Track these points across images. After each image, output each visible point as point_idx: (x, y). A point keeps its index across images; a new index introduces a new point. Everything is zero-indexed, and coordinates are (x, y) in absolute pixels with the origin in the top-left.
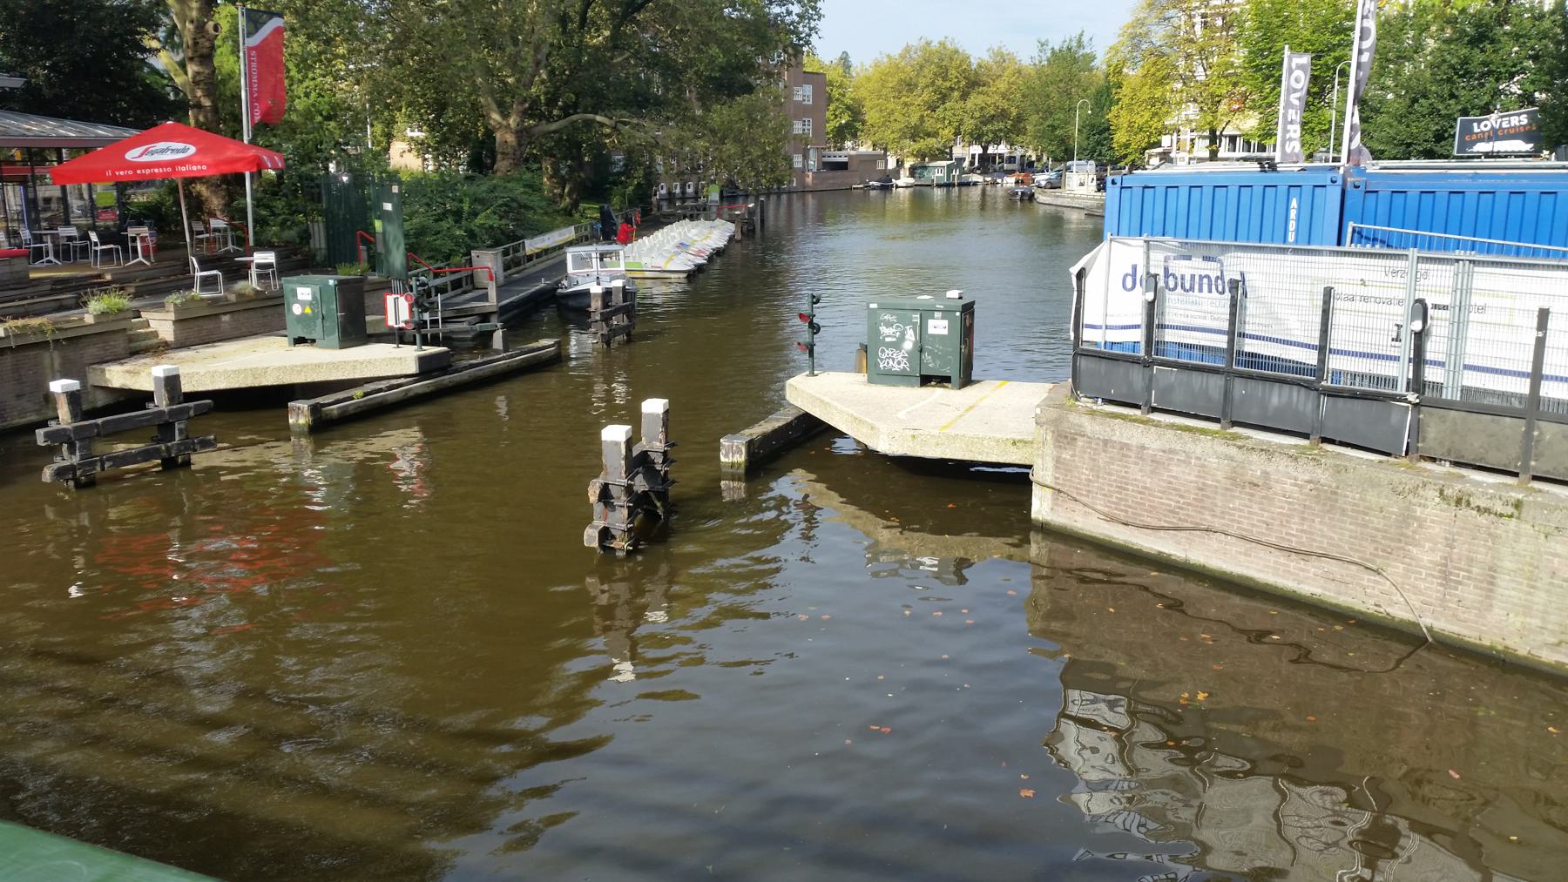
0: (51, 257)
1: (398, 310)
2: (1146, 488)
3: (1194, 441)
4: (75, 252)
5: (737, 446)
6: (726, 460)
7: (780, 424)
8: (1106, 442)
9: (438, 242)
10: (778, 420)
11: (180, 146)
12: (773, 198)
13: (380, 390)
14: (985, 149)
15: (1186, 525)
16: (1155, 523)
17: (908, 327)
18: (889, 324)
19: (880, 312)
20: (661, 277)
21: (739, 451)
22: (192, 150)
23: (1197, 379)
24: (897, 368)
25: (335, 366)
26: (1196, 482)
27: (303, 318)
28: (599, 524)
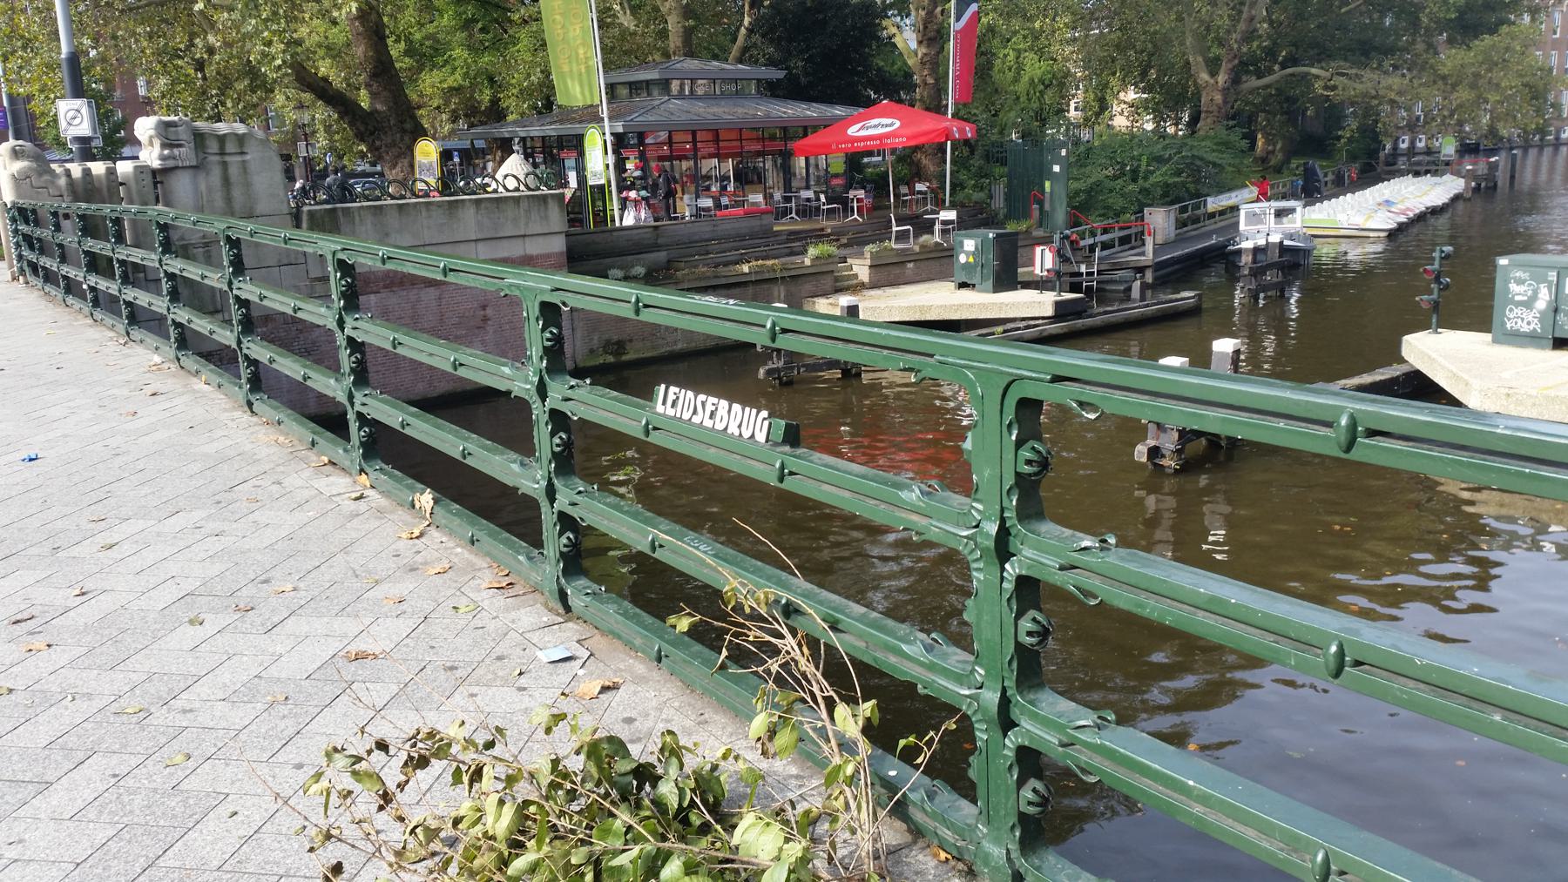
0: (794, 215)
1: (1044, 260)
4: (811, 211)
7: (1383, 378)
9: (1111, 201)
10: (1383, 374)
11: (888, 121)
12: (1533, 152)
13: (1019, 329)
17: (1542, 286)
18: (1520, 282)
19: (1510, 268)
20: (1359, 237)
22: (898, 124)
24: (1526, 328)
25: (984, 306)
27: (967, 265)
28: (1151, 442)
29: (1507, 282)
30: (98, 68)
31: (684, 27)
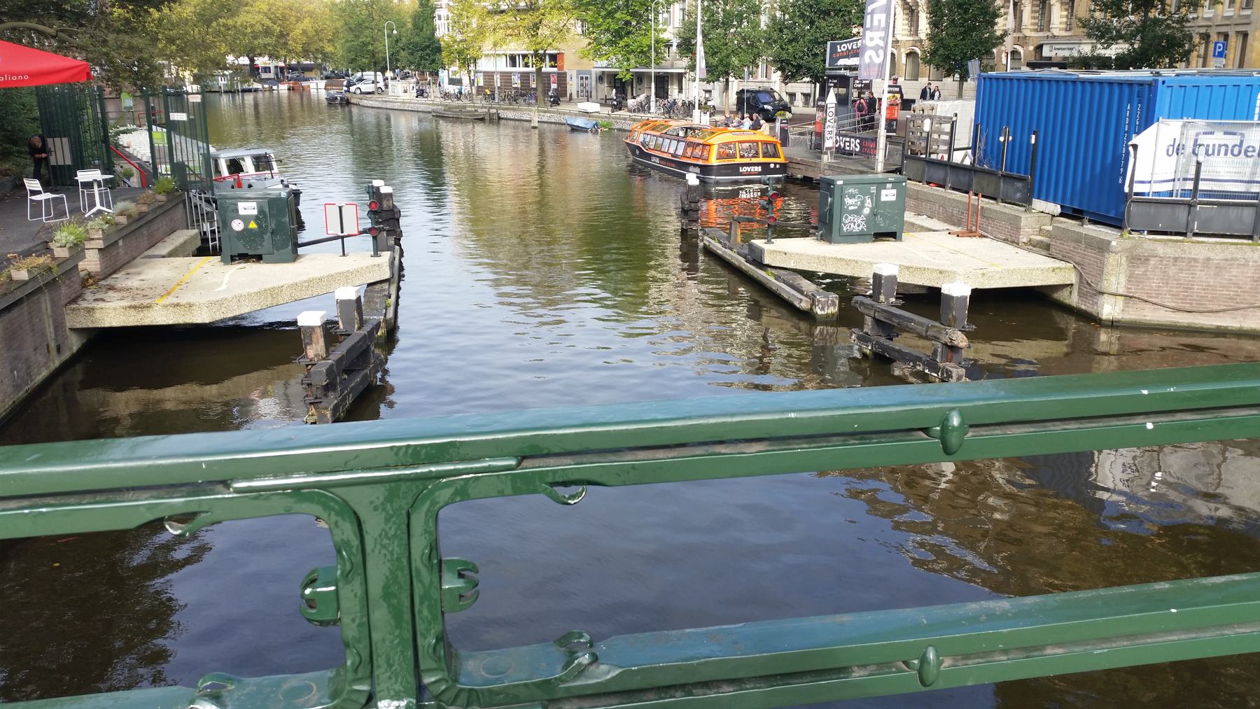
2: (1210, 286)
3: (1253, 251)
5: (832, 301)
6: (823, 313)
8: (1176, 259)
14: (252, 60)
15: (1242, 306)
16: (1215, 308)
18: (852, 196)
19: (844, 187)
21: (833, 304)
23: (1233, 212)
24: (857, 229)
26: (1253, 277)
29: (842, 198)
30: (544, 664)
31: (825, 101)
